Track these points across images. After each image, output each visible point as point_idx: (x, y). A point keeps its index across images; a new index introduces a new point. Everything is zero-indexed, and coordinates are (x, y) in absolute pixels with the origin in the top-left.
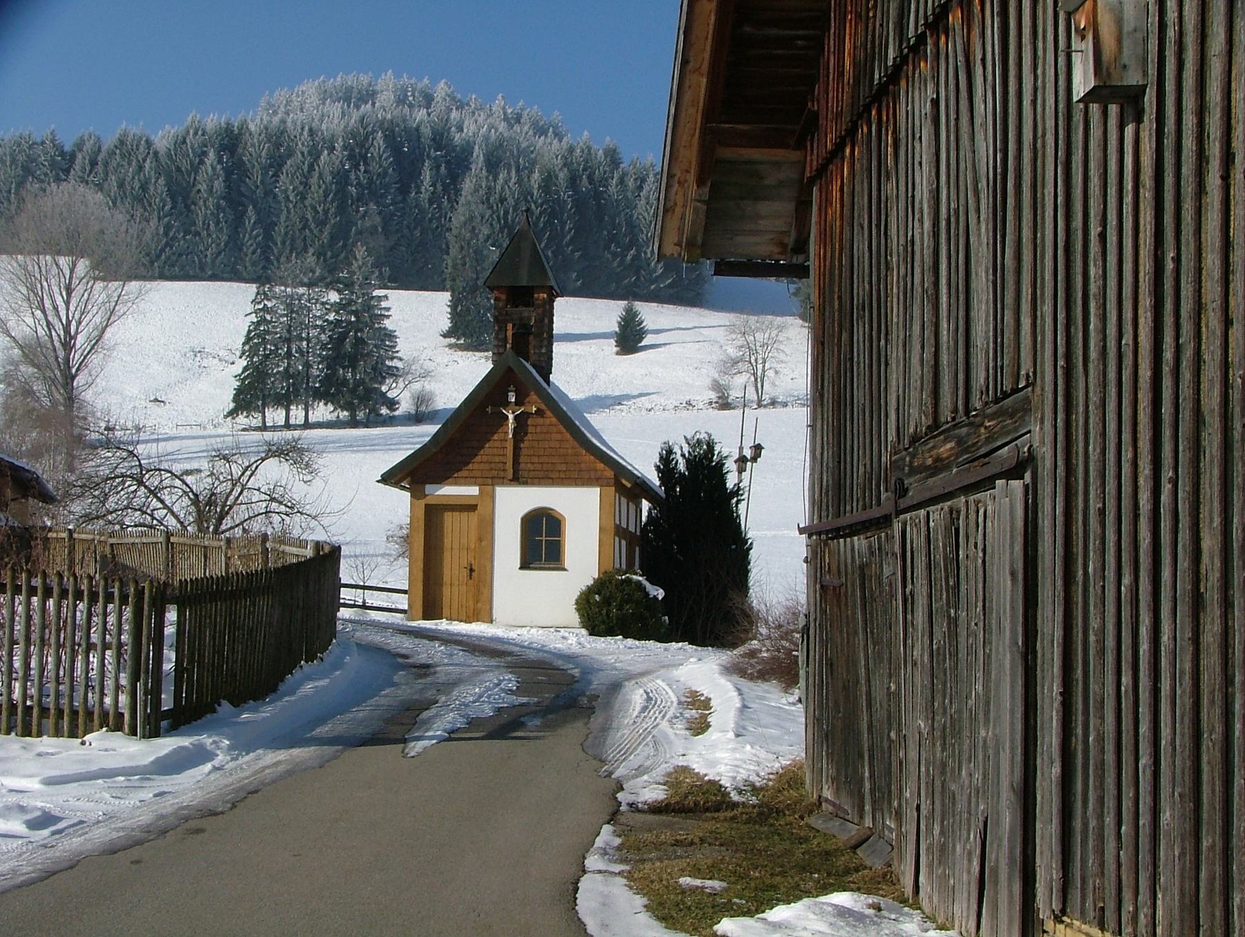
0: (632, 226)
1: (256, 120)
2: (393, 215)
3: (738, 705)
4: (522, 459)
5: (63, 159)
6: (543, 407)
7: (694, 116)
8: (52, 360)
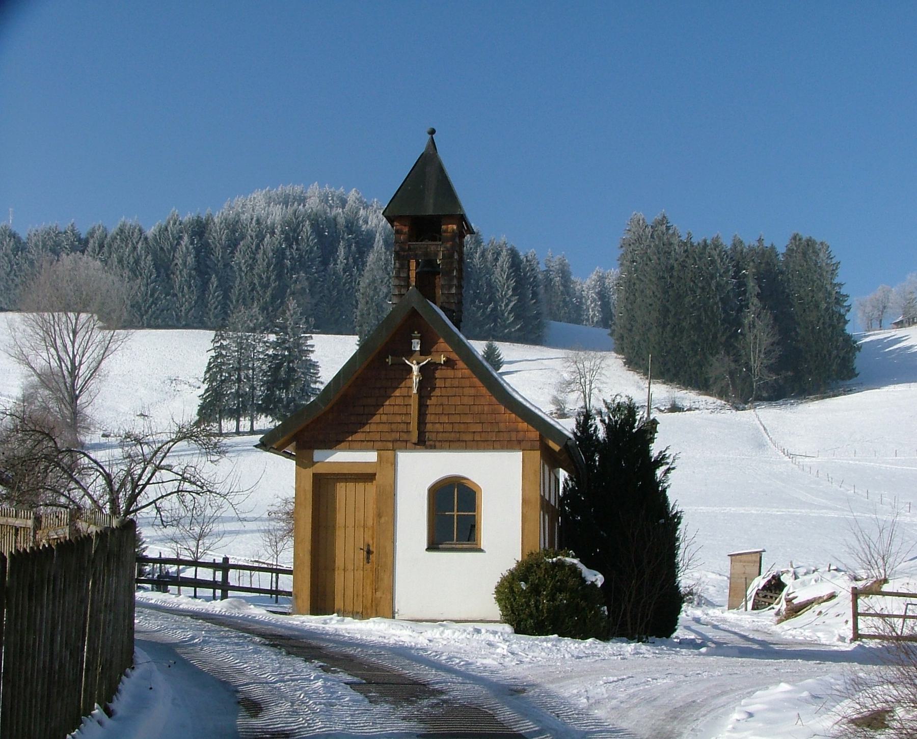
0: (490, 285)
2: (317, 280)
4: (429, 418)
5: (80, 243)
6: (454, 356)
8: (62, 386)
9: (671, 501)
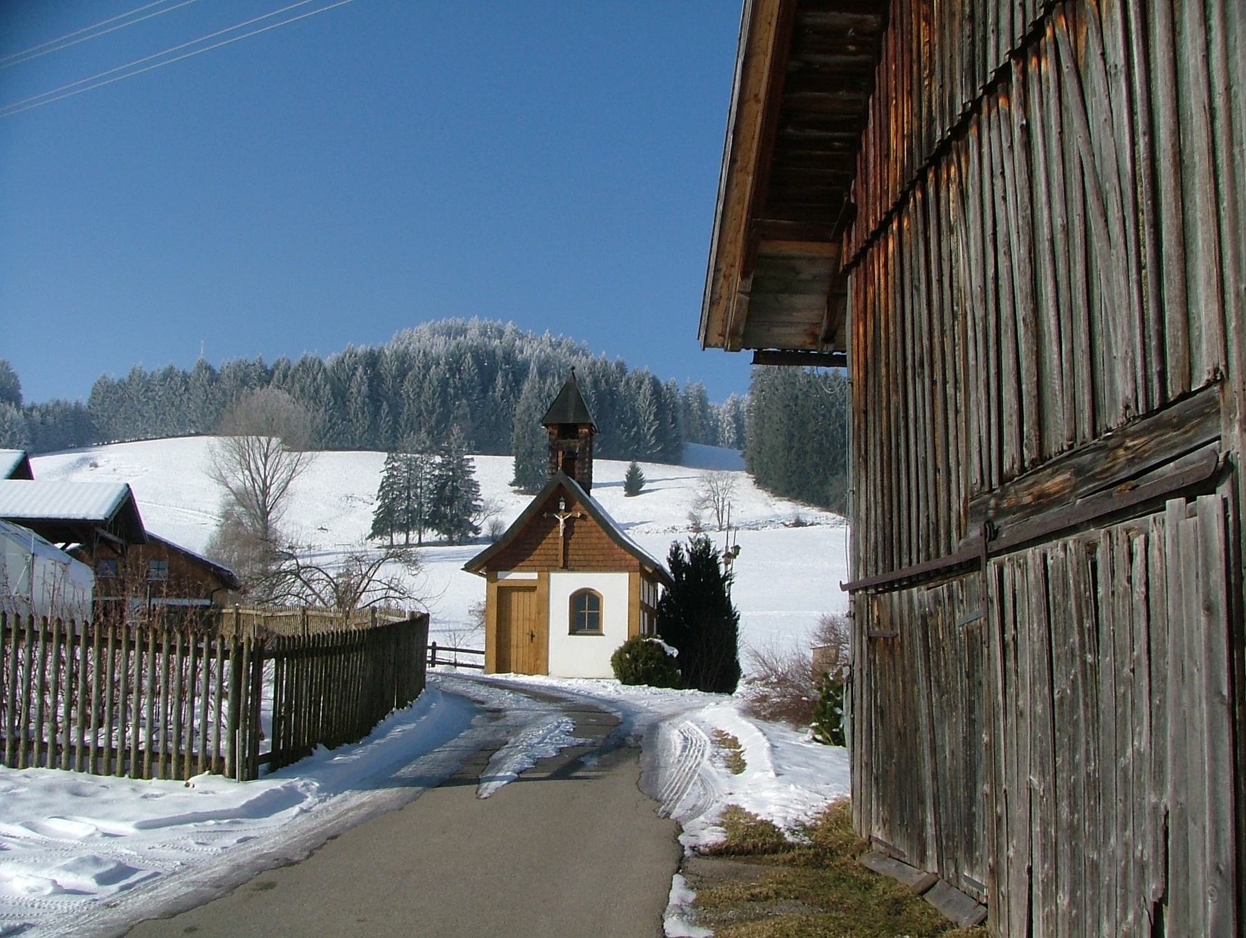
0: (633, 409)
1: (390, 348)
3: (768, 745)
6: (586, 513)
7: (741, 213)
8: (254, 502)
9: (733, 604)
